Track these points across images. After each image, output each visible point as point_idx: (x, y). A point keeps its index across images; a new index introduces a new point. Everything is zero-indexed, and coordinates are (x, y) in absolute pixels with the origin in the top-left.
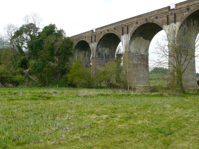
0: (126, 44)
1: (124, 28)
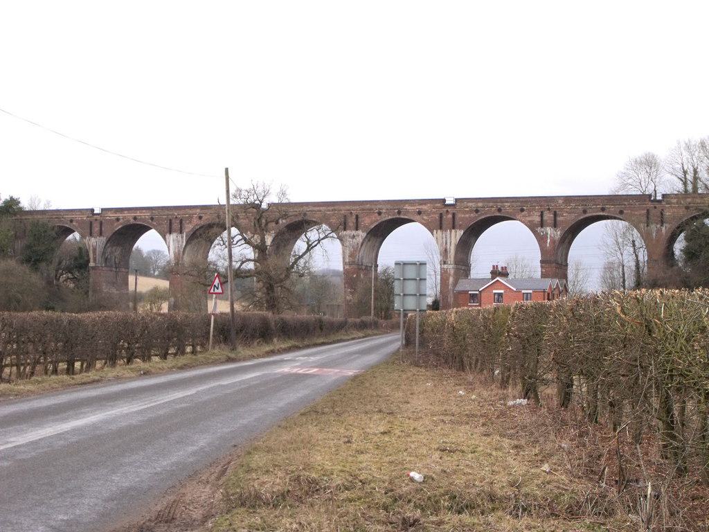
0: (177, 251)
1: (173, 221)
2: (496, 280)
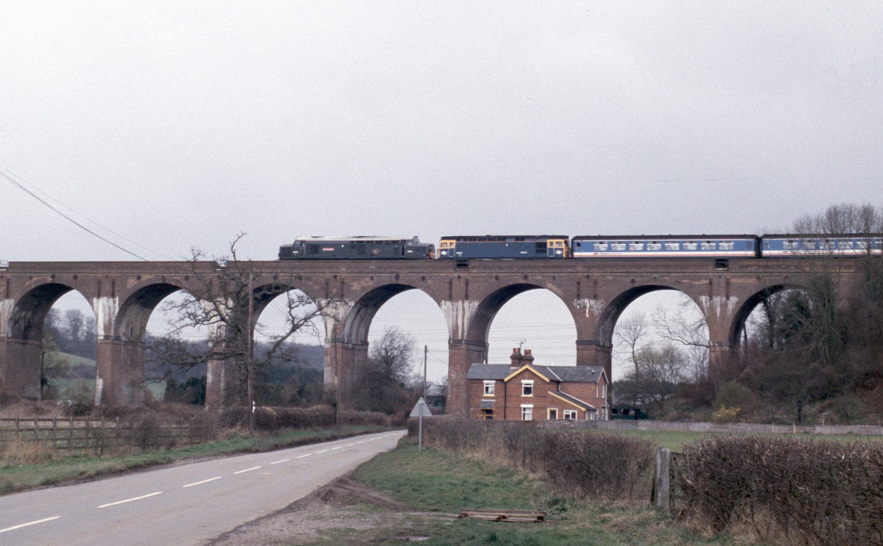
2: (524, 368)
